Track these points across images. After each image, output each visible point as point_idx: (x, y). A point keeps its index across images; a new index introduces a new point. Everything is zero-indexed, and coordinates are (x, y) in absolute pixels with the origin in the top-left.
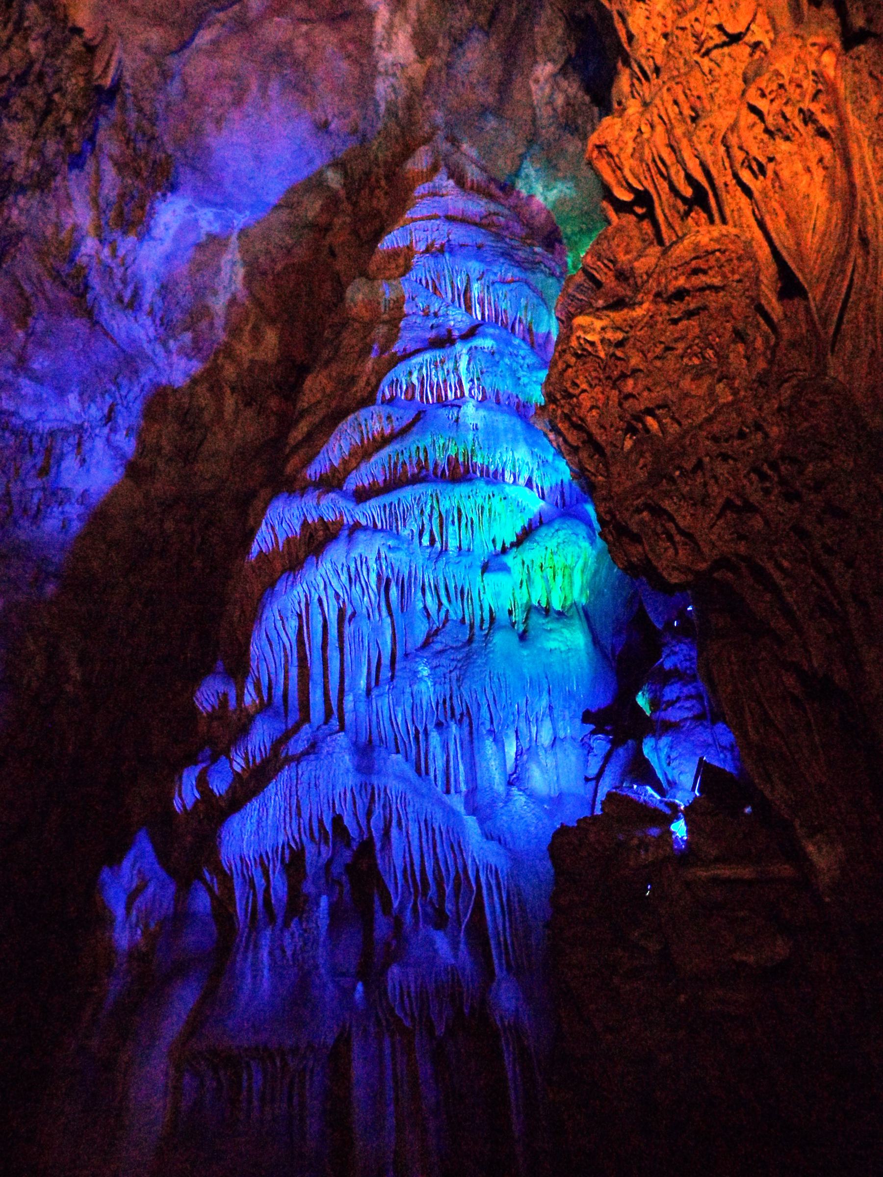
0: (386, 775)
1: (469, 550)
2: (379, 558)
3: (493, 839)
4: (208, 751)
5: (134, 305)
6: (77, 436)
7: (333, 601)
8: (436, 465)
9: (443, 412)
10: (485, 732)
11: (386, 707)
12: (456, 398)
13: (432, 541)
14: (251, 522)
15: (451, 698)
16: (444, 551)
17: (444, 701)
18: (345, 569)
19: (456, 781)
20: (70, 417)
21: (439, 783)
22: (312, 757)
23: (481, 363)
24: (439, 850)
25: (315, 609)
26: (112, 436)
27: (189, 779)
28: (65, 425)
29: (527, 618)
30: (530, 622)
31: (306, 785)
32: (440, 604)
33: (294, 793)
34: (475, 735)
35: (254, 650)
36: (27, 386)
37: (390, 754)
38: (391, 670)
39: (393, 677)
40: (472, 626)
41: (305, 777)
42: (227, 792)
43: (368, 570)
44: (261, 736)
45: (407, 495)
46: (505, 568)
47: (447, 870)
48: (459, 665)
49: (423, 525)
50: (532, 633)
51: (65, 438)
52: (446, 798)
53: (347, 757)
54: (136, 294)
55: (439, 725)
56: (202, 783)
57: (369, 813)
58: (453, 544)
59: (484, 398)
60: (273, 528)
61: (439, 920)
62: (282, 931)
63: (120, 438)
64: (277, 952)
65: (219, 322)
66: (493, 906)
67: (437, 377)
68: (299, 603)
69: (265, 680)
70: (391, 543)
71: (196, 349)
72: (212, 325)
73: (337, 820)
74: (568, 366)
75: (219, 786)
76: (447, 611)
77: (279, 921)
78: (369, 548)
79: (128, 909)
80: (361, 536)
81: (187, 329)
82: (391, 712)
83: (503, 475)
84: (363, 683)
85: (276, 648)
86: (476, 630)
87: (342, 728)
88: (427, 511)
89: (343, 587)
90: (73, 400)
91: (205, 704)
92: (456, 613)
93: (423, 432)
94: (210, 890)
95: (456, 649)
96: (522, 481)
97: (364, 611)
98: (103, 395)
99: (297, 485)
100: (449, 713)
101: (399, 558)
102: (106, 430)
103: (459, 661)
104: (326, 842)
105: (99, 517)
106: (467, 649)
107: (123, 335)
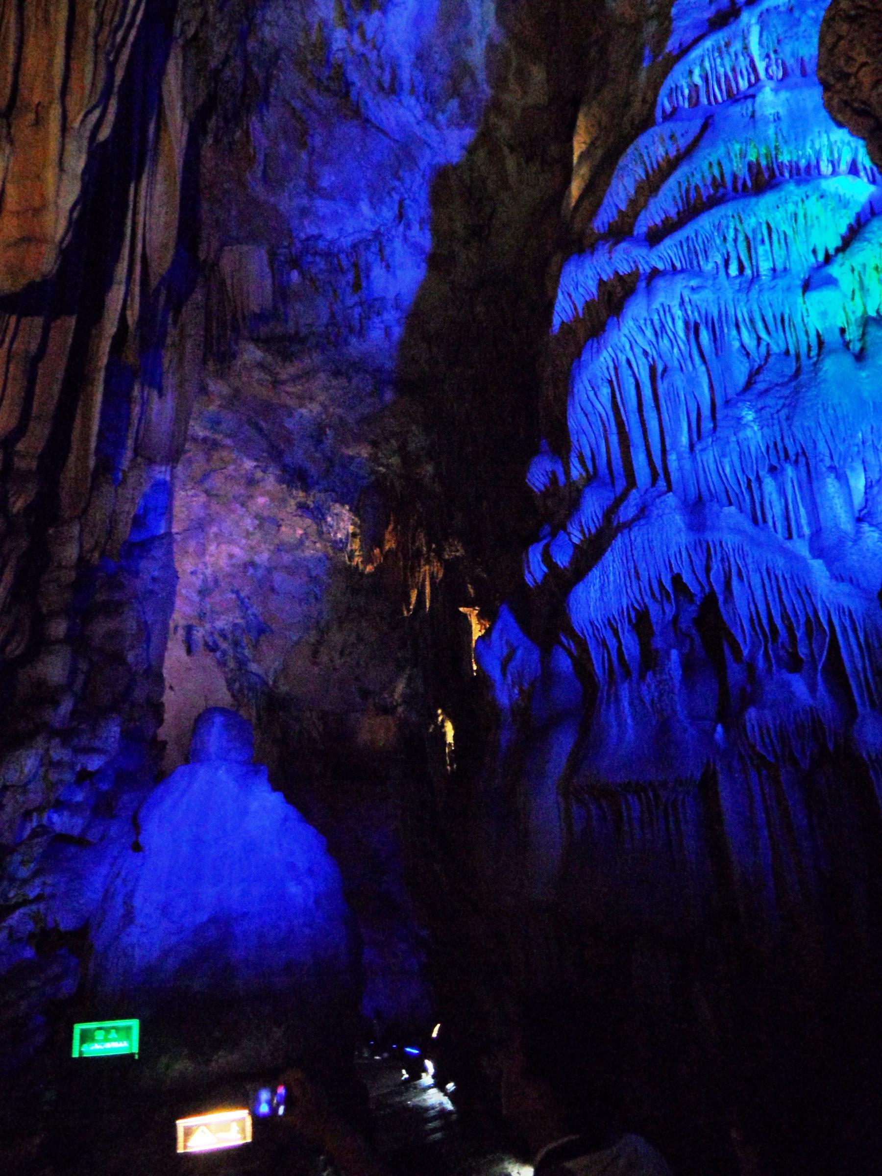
0: (720, 529)
1: (785, 269)
2: (682, 303)
3: (843, 580)
4: (547, 529)
5: (393, 90)
6: (377, 244)
7: (642, 360)
8: (735, 177)
9: (736, 110)
10: (824, 469)
11: (711, 460)
12: (751, 85)
13: (741, 268)
14: (550, 293)
15: (782, 439)
16: (756, 276)
17: (775, 444)
18: (649, 322)
19: (799, 526)
20: (368, 226)
21: (780, 530)
22: (642, 522)
23: (778, 26)
24: (784, 597)
25: (625, 372)
26: (408, 233)
27: (535, 556)
28: (364, 235)
29: (864, 334)
30: (868, 338)
31: (640, 549)
32: (759, 339)
33: (630, 558)
34: (813, 475)
35: (572, 424)
36: (322, 206)
37: (722, 506)
38: (714, 420)
39: (714, 429)
40: (798, 356)
41: (639, 540)
42: (570, 563)
43: (673, 319)
44: (592, 508)
45: (705, 223)
46: (831, 282)
47: (796, 615)
48: (787, 402)
49: (728, 253)
50: (870, 349)
51: (367, 248)
52: (788, 544)
53: (678, 517)
54: (394, 77)
55: (772, 470)
56: (547, 558)
57: (708, 569)
58: (765, 266)
59: (786, 74)
60: (570, 295)
61: (794, 664)
62: (638, 684)
63: (415, 233)
64: (636, 702)
65: (481, 76)
66: (849, 645)
67: (724, 67)
68: (608, 368)
69: (587, 453)
70: (693, 283)
71: (465, 117)
72: (475, 83)
73: (677, 579)
74: (840, 38)
75: (562, 559)
76: (768, 345)
77: (635, 675)
78: (670, 296)
79: (504, 674)
80: (661, 283)
81: (452, 97)
82: (718, 464)
83: (818, 166)
84: (684, 440)
85: (592, 419)
86: (803, 357)
87: (670, 489)
88: (731, 234)
89: (650, 343)
90: (365, 207)
91: (537, 484)
92: (778, 345)
93: (713, 144)
94: (568, 650)
95: (783, 385)
96: (843, 167)
97: (676, 363)
98: (389, 193)
99: (587, 242)
100: (782, 455)
101: (706, 299)
102: (401, 228)
103: (786, 398)
104: (668, 598)
105: (415, 318)
106: (793, 384)
107: (393, 123)
